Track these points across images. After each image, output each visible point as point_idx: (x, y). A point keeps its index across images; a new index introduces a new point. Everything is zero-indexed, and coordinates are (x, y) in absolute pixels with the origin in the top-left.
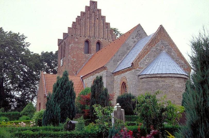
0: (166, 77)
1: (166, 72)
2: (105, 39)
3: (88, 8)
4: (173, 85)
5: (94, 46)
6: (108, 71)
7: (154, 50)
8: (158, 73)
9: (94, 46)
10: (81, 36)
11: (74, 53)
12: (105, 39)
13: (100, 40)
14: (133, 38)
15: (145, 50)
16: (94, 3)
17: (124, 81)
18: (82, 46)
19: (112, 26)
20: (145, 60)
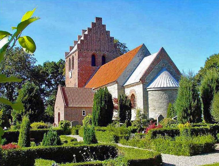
0: (166, 90)
1: (116, 89)
2: (110, 52)
3: (94, 24)
4: (172, 96)
5: (99, 60)
6: (119, 84)
7: (157, 68)
8: (158, 87)
9: (99, 60)
10: (88, 51)
11: (82, 66)
12: (110, 52)
13: (105, 53)
14: (138, 56)
15: (150, 68)
16: (99, 20)
17: (134, 93)
18: (90, 59)
19: (111, 35)
20: (150, 77)
